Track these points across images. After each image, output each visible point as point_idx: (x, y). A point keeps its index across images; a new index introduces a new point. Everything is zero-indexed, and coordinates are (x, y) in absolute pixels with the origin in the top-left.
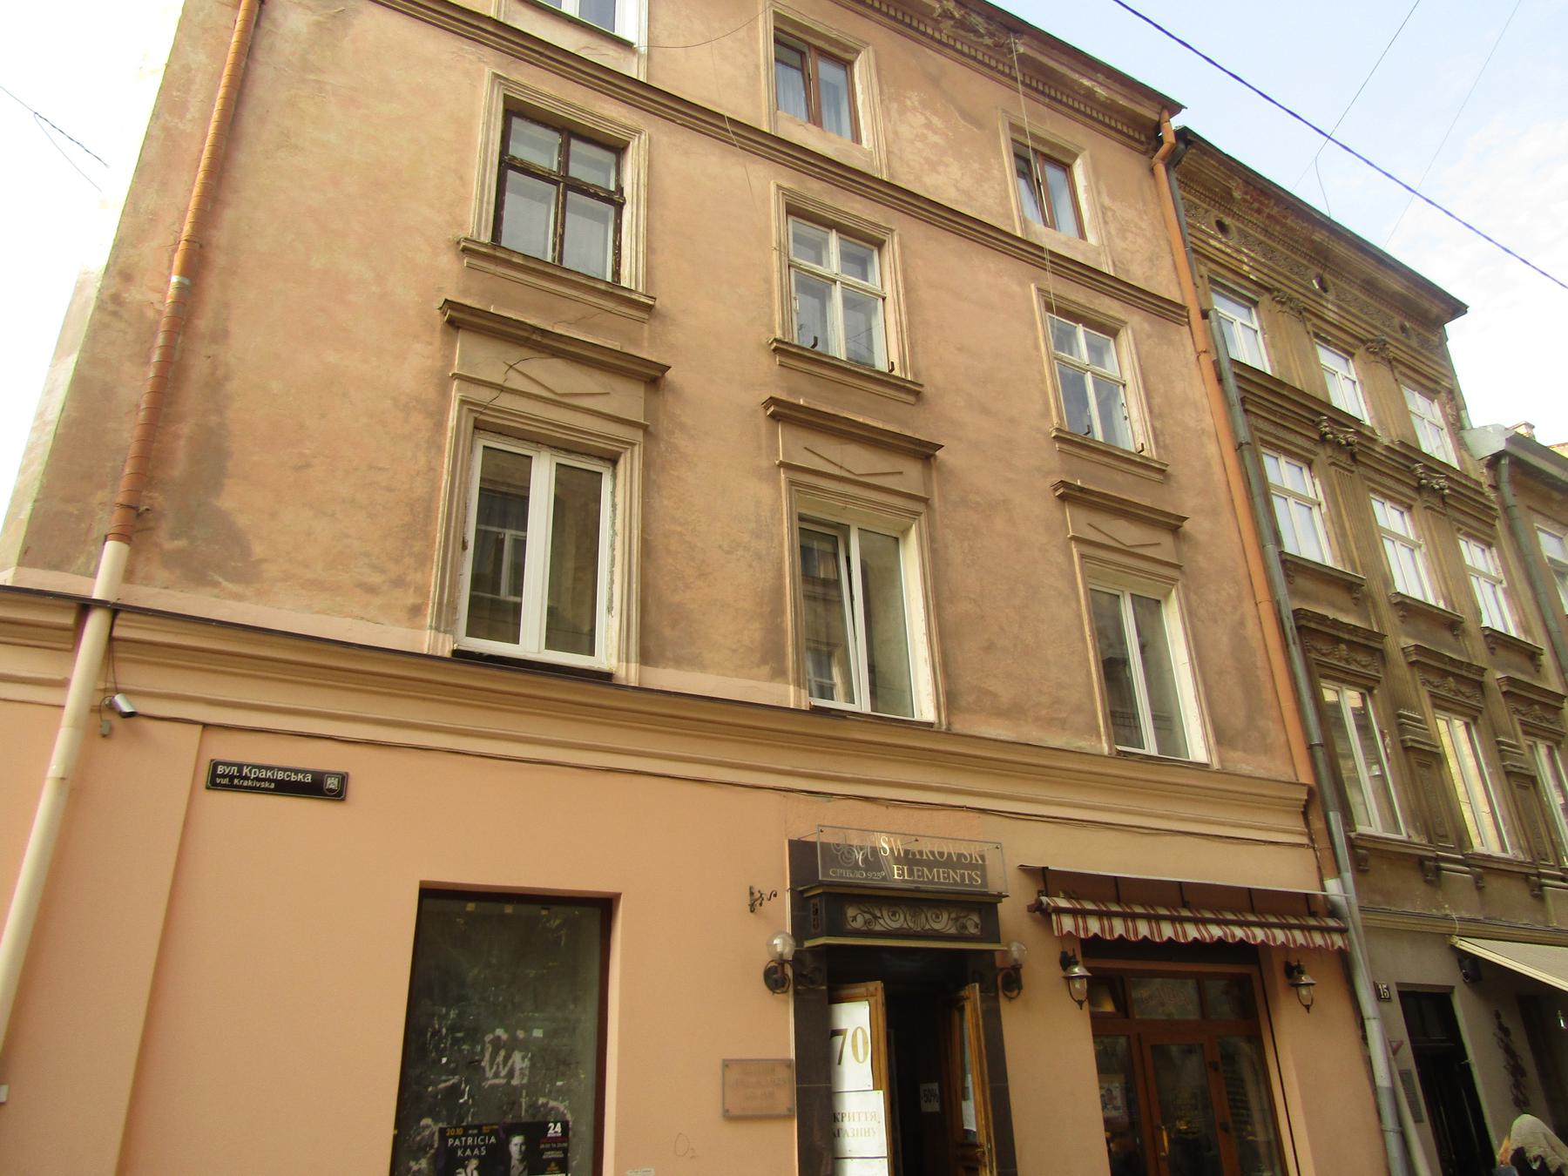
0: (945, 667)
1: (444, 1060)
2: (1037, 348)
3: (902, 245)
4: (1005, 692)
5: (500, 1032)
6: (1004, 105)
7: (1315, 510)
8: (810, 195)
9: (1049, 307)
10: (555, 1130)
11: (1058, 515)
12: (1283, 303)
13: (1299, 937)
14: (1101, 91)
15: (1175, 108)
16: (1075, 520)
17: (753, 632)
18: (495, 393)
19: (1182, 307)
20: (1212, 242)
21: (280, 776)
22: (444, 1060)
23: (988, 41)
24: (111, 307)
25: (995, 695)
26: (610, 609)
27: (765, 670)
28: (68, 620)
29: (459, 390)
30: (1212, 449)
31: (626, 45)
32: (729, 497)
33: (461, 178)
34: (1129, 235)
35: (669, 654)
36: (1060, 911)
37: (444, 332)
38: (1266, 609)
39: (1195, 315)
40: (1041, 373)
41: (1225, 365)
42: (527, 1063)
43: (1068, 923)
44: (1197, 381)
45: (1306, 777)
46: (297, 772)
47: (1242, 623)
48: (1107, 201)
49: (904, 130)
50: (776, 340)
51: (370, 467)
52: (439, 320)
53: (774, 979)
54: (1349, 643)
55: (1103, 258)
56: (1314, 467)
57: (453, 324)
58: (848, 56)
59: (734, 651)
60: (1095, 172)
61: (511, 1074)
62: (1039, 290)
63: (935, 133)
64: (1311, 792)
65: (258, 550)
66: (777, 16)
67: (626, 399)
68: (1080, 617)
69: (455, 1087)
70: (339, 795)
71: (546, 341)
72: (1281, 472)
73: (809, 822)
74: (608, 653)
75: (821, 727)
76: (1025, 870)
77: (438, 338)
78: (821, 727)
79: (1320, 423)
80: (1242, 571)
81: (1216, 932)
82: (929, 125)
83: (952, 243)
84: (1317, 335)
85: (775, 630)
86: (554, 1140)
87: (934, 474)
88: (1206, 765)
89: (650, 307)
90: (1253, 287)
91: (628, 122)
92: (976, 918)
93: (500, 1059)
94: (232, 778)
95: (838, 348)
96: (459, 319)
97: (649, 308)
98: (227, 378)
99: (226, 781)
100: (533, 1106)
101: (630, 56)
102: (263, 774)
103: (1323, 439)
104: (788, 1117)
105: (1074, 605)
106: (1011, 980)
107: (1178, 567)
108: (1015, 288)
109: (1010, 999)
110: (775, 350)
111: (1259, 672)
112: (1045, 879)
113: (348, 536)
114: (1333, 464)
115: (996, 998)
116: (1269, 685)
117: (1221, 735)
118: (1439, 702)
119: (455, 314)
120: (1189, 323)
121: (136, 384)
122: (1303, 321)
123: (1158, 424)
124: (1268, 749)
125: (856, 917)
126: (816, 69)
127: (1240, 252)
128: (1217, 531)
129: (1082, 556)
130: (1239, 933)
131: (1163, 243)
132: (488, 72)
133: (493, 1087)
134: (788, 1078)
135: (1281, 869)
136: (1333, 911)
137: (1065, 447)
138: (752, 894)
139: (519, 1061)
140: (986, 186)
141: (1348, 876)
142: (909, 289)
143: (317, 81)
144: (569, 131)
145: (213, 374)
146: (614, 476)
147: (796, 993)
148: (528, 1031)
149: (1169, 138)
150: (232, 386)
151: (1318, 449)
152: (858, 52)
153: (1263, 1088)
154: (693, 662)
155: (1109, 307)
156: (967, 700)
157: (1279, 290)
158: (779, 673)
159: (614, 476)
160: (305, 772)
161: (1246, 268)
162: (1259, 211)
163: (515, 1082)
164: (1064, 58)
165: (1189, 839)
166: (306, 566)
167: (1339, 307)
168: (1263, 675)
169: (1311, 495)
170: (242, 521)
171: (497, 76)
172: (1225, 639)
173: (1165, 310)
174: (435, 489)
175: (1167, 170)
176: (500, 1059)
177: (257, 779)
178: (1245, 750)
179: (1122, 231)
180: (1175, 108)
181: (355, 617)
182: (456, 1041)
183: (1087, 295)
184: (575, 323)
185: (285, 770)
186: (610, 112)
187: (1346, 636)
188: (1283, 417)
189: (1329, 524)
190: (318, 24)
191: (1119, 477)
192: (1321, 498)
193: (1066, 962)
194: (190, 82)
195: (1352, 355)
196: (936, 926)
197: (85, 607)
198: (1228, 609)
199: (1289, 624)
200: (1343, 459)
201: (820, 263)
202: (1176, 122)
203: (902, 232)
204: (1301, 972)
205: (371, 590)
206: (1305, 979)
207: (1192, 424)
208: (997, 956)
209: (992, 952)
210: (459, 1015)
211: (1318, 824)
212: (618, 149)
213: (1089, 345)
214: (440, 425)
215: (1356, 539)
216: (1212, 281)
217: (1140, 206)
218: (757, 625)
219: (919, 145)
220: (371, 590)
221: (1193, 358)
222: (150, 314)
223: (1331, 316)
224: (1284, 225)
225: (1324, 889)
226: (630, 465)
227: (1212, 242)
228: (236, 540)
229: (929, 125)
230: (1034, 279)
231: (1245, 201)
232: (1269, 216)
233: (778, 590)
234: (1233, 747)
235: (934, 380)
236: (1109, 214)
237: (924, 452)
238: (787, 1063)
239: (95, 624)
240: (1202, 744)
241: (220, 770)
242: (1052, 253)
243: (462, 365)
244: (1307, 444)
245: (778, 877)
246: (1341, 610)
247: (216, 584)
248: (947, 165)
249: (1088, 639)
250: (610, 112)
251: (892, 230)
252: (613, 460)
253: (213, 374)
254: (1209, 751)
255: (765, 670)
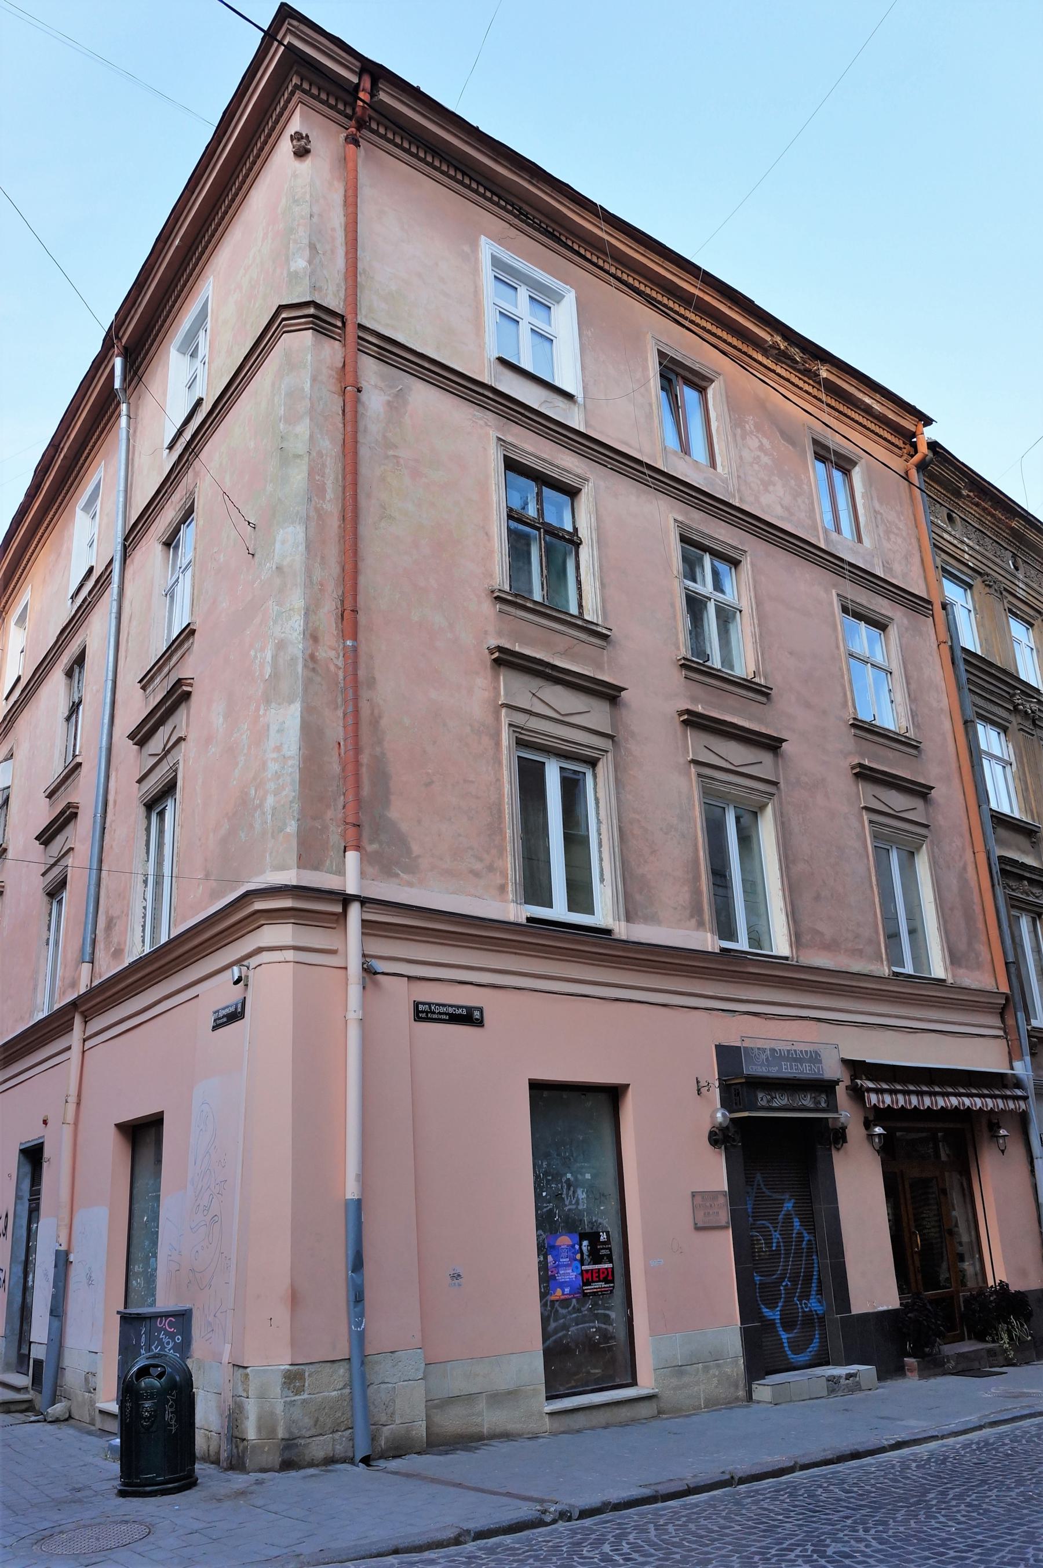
0: (793, 915)
1: (544, 1194)
2: (838, 647)
3: (753, 564)
4: (827, 930)
5: (569, 1176)
6: (800, 411)
7: (1008, 768)
8: (695, 526)
9: (845, 610)
10: (603, 1237)
11: (854, 789)
12: (990, 586)
13: (1000, 1103)
14: (876, 406)
15: (928, 421)
16: (867, 794)
17: (684, 896)
18: (527, 716)
19: (929, 602)
20: (946, 536)
21: (451, 1010)
22: (544, 1194)
23: (802, 368)
24: (311, 665)
25: (822, 934)
26: (602, 880)
27: (693, 921)
28: (338, 909)
29: (507, 715)
30: (947, 725)
31: (569, 396)
32: (650, 785)
33: (487, 534)
34: (892, 536)
35: (640, 913)
36: (869, 1090)
37: (492, 668)
38: (982, 858)
39: (937, 607)
40: (841, 669)
41: (959, 653)
42: (585, 1195)
43: (874, 1098)
44: (938, 667)
45: (1005, 989)
46: (458, 1007)
47: (965, 868)
48: (877, 506)
49: (747, 455)
50: (684, 658)
51: (465, 781)
52: (488, 659)
53: (718, 1138)
54: (1031, 881)
55: (876, 560)
56: (1009, 732)
57: (498, 662)
58: (704, 384)
59: (676, 909)
60: (870, 481)
61: (577, 1203)
62: (838, 595)
63: (766, 454)
64: (1007, 999)
65: (416, 849)
66: (661, 354)
67: (595, 714)
68: (869, 869)
69: (551, 1210)
70: (479, 1023)
71: (554, 673)
72: (989, 738)
73: (735, 1032)
74: (604, 913)
75: (728, 967)
76: (845, 1061)
77: (489, 672)
78: (728, 967)
79: (1014, 695)
80: (966, 827)
81: (954, 1101)
82: (761, 447)
83: (782, 558)
84: (1010, 611)
85: (697, 892)
86: (604, 1243)
87: (780, 761)
88: (944, 981)
89: (608, 636)
90: (970, 572)
91: (579, 471)
92: (824, 1096)
93: (571, 1193)
94: (427, 1013)
95: (716, 662)
96: (506, 660)
97: (605, 637)
98: (380, 717)
99: (424, 1015)
100: (590, 1222)
101: (572, 406)
102: (443, 1010)
103: (1016, 710)
104: (726, 1228)
105: (866, 861)
106: (839, 1136)
107: (927, 826)
108: (823, 595)
109: (838, 1149)
110: (682, 665)
111: (975, 907)
112: (856, 1068)
113: (460, 835)
114: (1022, 730)
115: (830, 1150)
116: (981, 917)
117: (954, 958)
118: (1022, 891)
119: (502, 656)
120: (933, 616)
121: (335, 729)
122: (1002, 598)
123: (914, 707)
124: (979, 966)
125: (762, 1099)
126: (682, 391)
127: (963, 542)
128: (949, 795)
129: (871, 822)
130: (967, 1101)
131: (914, 541)
132: (493, 434)
133: (569, 1210)
134: (723, 1201)
135: (985, 1056)
136: (1018, 1084)
137: (858, 732)
138: (698, 1082)
139: (581, 1194)
140: (800, 500)
141: (1028, 1058)
142: (759, 604)
143: (394, 456)
144: (542, 480)
145: (372, 714)
146: (595, 776)
147: (726, 1148)
148: (583, 1174)
149: (923, 449)
150: (384, 722)
151: (1012, 718)
152: (712, 381)
153: (969, 1207)
154: (651, 919)
155: (881, 606)
156: (806, 938)
157: (988, 575)
158: (701, 924)
159: (595, 776)
160: (462, 1007)
161: (967, 556)
162: (977, 505)
163: (580, 1207)
164: (854, 382)
165: (933, 1035)
166: (441, 859)
167: (1027, 584)
168: (977, 908)
169: (1006, 758)
170: (404, 827)
171: (499, 439)
172: (955, 882)
173: (918, 605)
174: (501, 796)
175: (918, 472)
176: (571, 1193)
177: (440, 1013)
178: (967, 967)
179: (887, 532)
180: (928, 421)
181: (472, 895)
182: (548, 1181)
183: (871, 596)
184: (565, 654)
185: (451, 1006)
186: (566, 463)
187: (1028, 875)
188: (992, 693)
189: (1017, 781)
190: (389, 403)
191: (890, 754)
192: (1013, 759)
193: (868, 1125)
194: (324, 465)
195: (1032, 625)
196: (805, 1103)
197: (346, 900)
198: (957, 858)
199: (996, 868)
200: (1028, 724)
201: (694, 581)
202: (930, 433)
203: (756, 553)
204: (1000, 1127)
205: (476, 874)
206: (1003, 1132)
207: (935, 704)
208: (830, 1121)
209: (827, 1118)
210: (548, 1165)
211: (1010, 1022)
212: (572, 493)
213: (868, 637)
214: (498, 744)
215: (1034, 792)
216: (944, 570)
217: (898, 508)
218: (686, 888)
219: (756, 467)
220: (476, 874)
221: (935, 646)
222: (332, 668)
223: (1021, 593)
224: (993, 516)
225: (1012, 1068)
226: (604, 767)
227: (946, 536)
228: (401, 840)
229: (761, 447)
230: (835, 586)
231: (968, 496)
232: (984, 509)
233: (696, 861)
234: (960, 966)
235: (776, 681)
236: (879, 517)
237: (772, 745)
238: (723, 1193)
239: (355, 912)
240: (941, 964)
241: (421, 1007)
242: (850, 564)
243: (506, 694)
244: (1004, 714)
245: (711, 1073)
246: (1024, 852)
247: (397, 875)
248: (774, 485)
249: (875, 887)
250: (566, 463)
251: (745, 552)
252: (593, 763)
253: (372, 714)
254: (946, 969)
255: (693, 921)
